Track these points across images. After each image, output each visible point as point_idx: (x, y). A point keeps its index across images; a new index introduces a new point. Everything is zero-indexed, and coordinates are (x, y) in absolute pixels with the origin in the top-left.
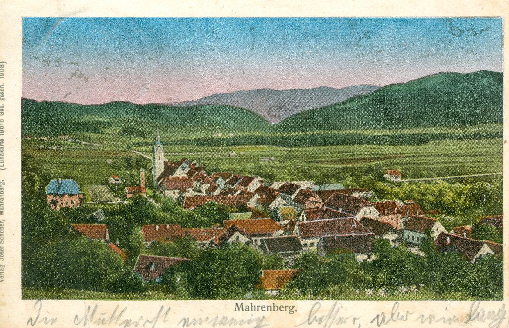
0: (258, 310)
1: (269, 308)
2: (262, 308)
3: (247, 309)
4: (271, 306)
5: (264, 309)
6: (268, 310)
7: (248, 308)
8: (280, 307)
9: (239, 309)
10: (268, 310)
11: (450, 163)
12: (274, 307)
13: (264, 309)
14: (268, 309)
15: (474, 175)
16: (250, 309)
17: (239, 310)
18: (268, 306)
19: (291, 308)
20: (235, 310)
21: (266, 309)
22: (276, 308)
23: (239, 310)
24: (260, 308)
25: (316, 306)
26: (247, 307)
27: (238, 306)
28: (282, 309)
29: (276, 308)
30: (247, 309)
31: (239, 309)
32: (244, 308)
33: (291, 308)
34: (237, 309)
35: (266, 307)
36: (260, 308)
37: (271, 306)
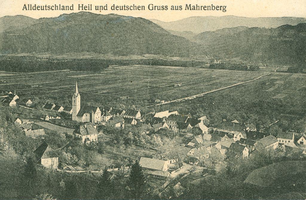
0: (201, 10)
1: (209, 7)
2: (204, 8)
3: (63, 9)
4: (210, 6)
5: (205, 9)
6: (142, 9)
7: (194, 8)
8: (217, 7)
9: (188, 9)
10: (142, 9)
11: (150, 67)
12: (212, 7)
13: (205, 9)
14: (221, 9)
15: (236, 85)
16: (200, 9)
17: (188, 10)
18: (142, 7)
19: (224, 7)
20: (186, 9)
21: (141, 8)
22: (213, 8)
23: (188, 10)
24: (202, 8)
25: (240, 73)
26: (194, 7)
27: (188, 7)
28: (139, 8)
29: (213, 8)
30: (193, 9)
31: (188, 9)
32: (192, 8)
33: (224, 7)
34: (187, 8)
35: (141, 7)
36: (202, 8)
37: (210, 6)
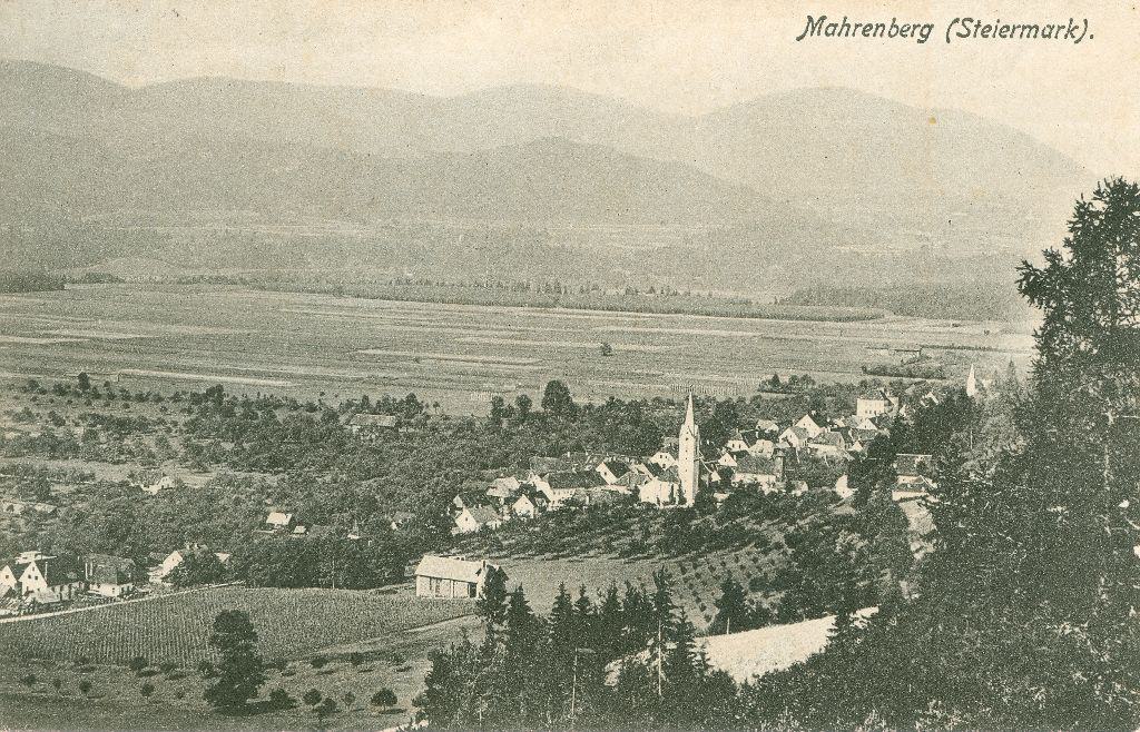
24: (860, 29)
